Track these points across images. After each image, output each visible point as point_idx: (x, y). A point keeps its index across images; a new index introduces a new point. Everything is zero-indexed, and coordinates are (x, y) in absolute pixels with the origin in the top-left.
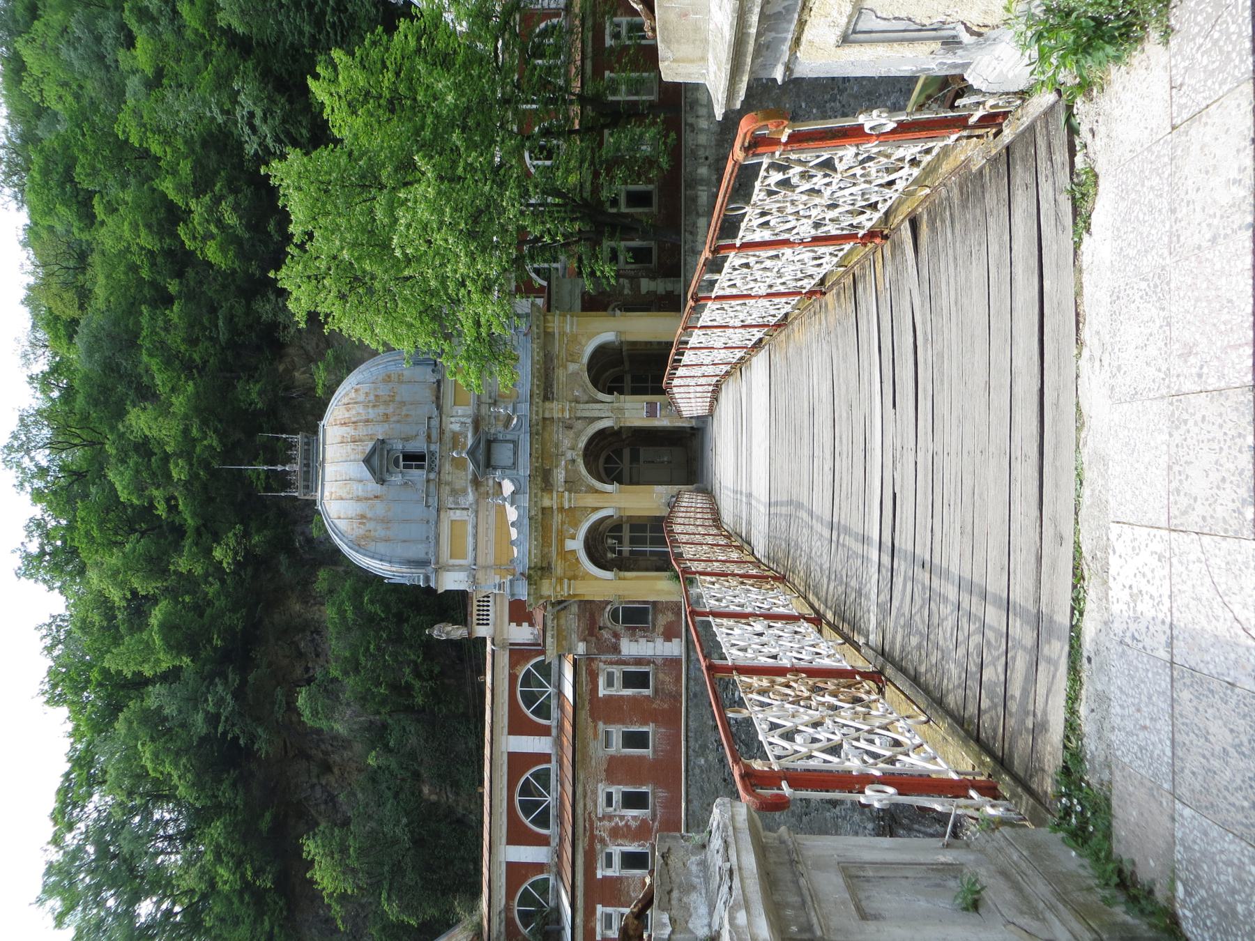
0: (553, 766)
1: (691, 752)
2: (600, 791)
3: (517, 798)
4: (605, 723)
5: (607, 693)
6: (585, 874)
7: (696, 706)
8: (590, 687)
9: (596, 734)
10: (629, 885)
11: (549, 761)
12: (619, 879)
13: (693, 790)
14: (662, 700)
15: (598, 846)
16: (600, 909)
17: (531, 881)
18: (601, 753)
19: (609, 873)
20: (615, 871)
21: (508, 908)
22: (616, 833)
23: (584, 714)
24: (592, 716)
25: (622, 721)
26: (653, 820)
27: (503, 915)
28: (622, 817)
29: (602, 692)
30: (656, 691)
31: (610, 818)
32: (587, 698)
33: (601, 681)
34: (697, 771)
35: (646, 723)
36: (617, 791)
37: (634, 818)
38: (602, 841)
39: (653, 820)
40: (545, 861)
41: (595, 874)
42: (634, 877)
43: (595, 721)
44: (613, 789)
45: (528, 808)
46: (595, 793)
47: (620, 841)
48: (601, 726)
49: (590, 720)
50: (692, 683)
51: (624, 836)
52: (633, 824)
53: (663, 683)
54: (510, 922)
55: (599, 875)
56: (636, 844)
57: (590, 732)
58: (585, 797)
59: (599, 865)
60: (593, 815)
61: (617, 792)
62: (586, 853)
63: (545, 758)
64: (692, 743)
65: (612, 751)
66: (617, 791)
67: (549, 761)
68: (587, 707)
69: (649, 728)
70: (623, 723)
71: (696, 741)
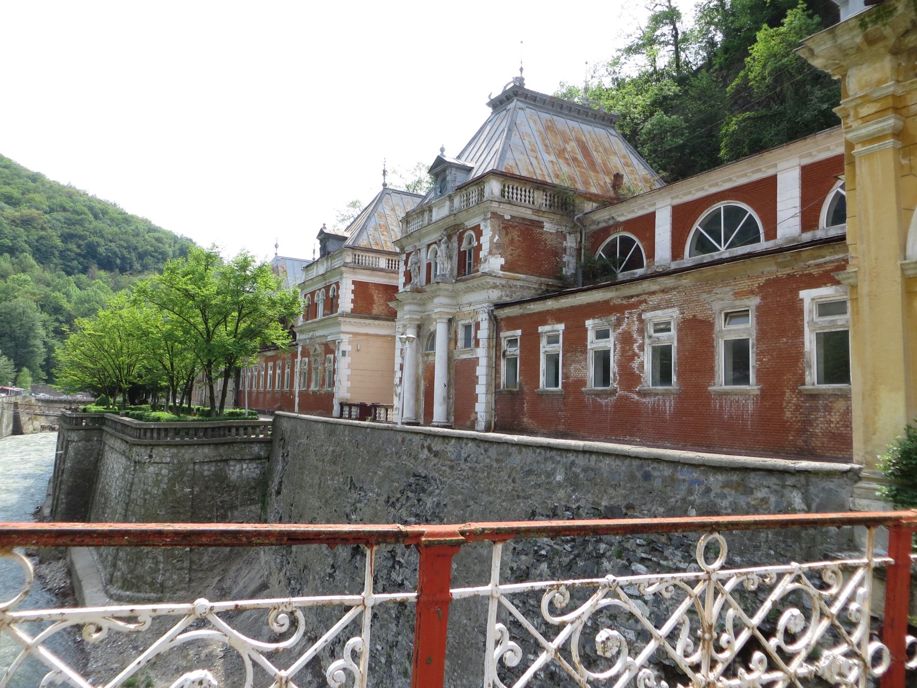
0: (763, 245)
1: (571, 457)
2: (669, 311)
3: (721, 205)
4: (758, 308)
5: (807, 306)
6: (589, 305)
7: (632, 478)
8: (815, 272)
9: (738, 295)
10: (579, 362)
11: (768, 238)
12: (584, 351)
13: (529, 455)
14: (798, 407)
15: (613, 318)
16: (561, 327)
17: (641, 246)
18: (717, 306)
19: (591, 335)
20: (593, 344)
21: (617, 226)
22: (626, 340)
23: (770, 269)
24: (769, 283)
25: (762, 335)
26: (639, 393)
27: (611, 222)
28: (642, 348)
29: (808, 296)
30: (813, 396)
31: (641, 331)
32: (797, 269)
33: (827, 292)
34: (549, 466)
35: (759, 380)
36: (670, 338)
37: (642, 365)
38: (619, 323)
39: (639, 393)
40: (656, 259)
41: (589, 319)
42: (586, 367)
43: (762, 290)
44: (673, 333)
45: (712, 225)
46: (669, 305)
47: (618, 347)
48: (753, 302)
49: (762, 280)
50: (667, 471)
51: (623, 351)
52: (635, 364)
53: (828, 409)
54: (606, 231)
55: (589, 323)
56: (616, 369)
57: (745, 285)
58: (663, 291)
59: (596, 321)
60: (643, 306)
61: (670, 338)
62: (607, 302)
63: (771, 234)
64: (581, 461)
65: (720, 323)
66: (670, 338)
67: (768, 238)
68: (783, 272)
69: (753, 387)
70: (759, 340)
71: (585, 470)
